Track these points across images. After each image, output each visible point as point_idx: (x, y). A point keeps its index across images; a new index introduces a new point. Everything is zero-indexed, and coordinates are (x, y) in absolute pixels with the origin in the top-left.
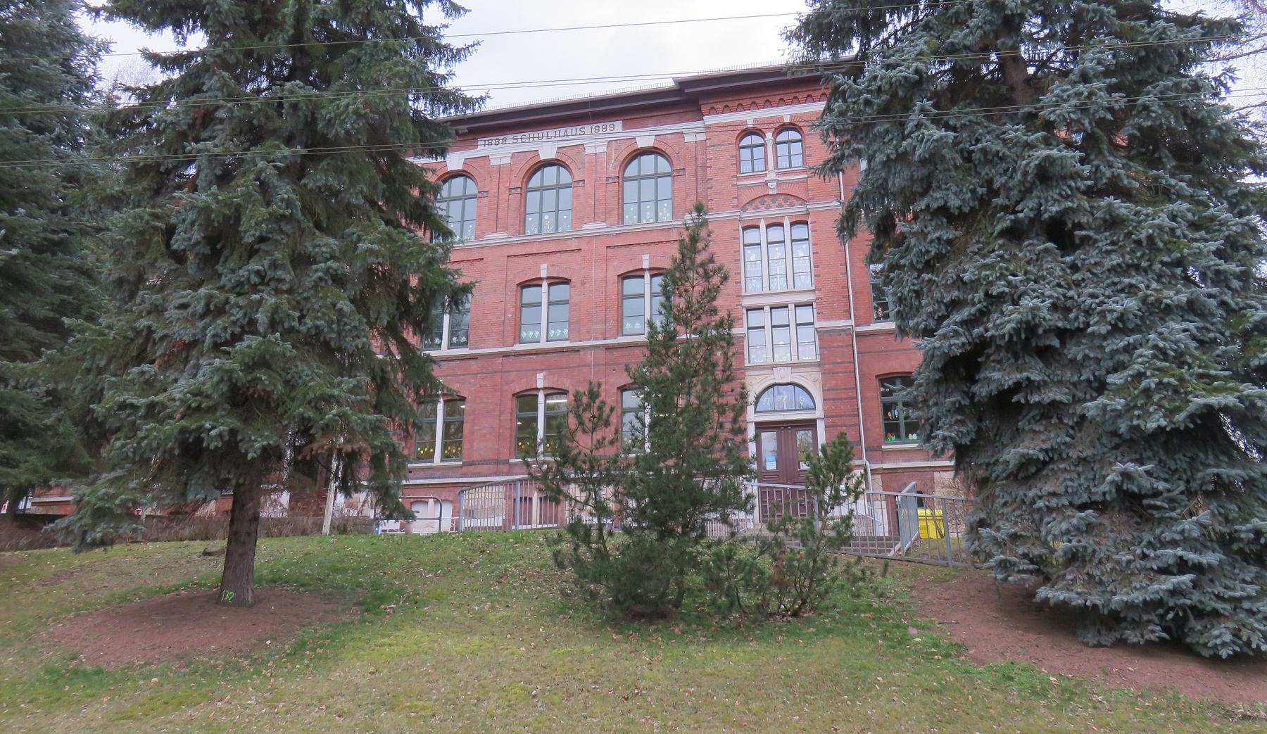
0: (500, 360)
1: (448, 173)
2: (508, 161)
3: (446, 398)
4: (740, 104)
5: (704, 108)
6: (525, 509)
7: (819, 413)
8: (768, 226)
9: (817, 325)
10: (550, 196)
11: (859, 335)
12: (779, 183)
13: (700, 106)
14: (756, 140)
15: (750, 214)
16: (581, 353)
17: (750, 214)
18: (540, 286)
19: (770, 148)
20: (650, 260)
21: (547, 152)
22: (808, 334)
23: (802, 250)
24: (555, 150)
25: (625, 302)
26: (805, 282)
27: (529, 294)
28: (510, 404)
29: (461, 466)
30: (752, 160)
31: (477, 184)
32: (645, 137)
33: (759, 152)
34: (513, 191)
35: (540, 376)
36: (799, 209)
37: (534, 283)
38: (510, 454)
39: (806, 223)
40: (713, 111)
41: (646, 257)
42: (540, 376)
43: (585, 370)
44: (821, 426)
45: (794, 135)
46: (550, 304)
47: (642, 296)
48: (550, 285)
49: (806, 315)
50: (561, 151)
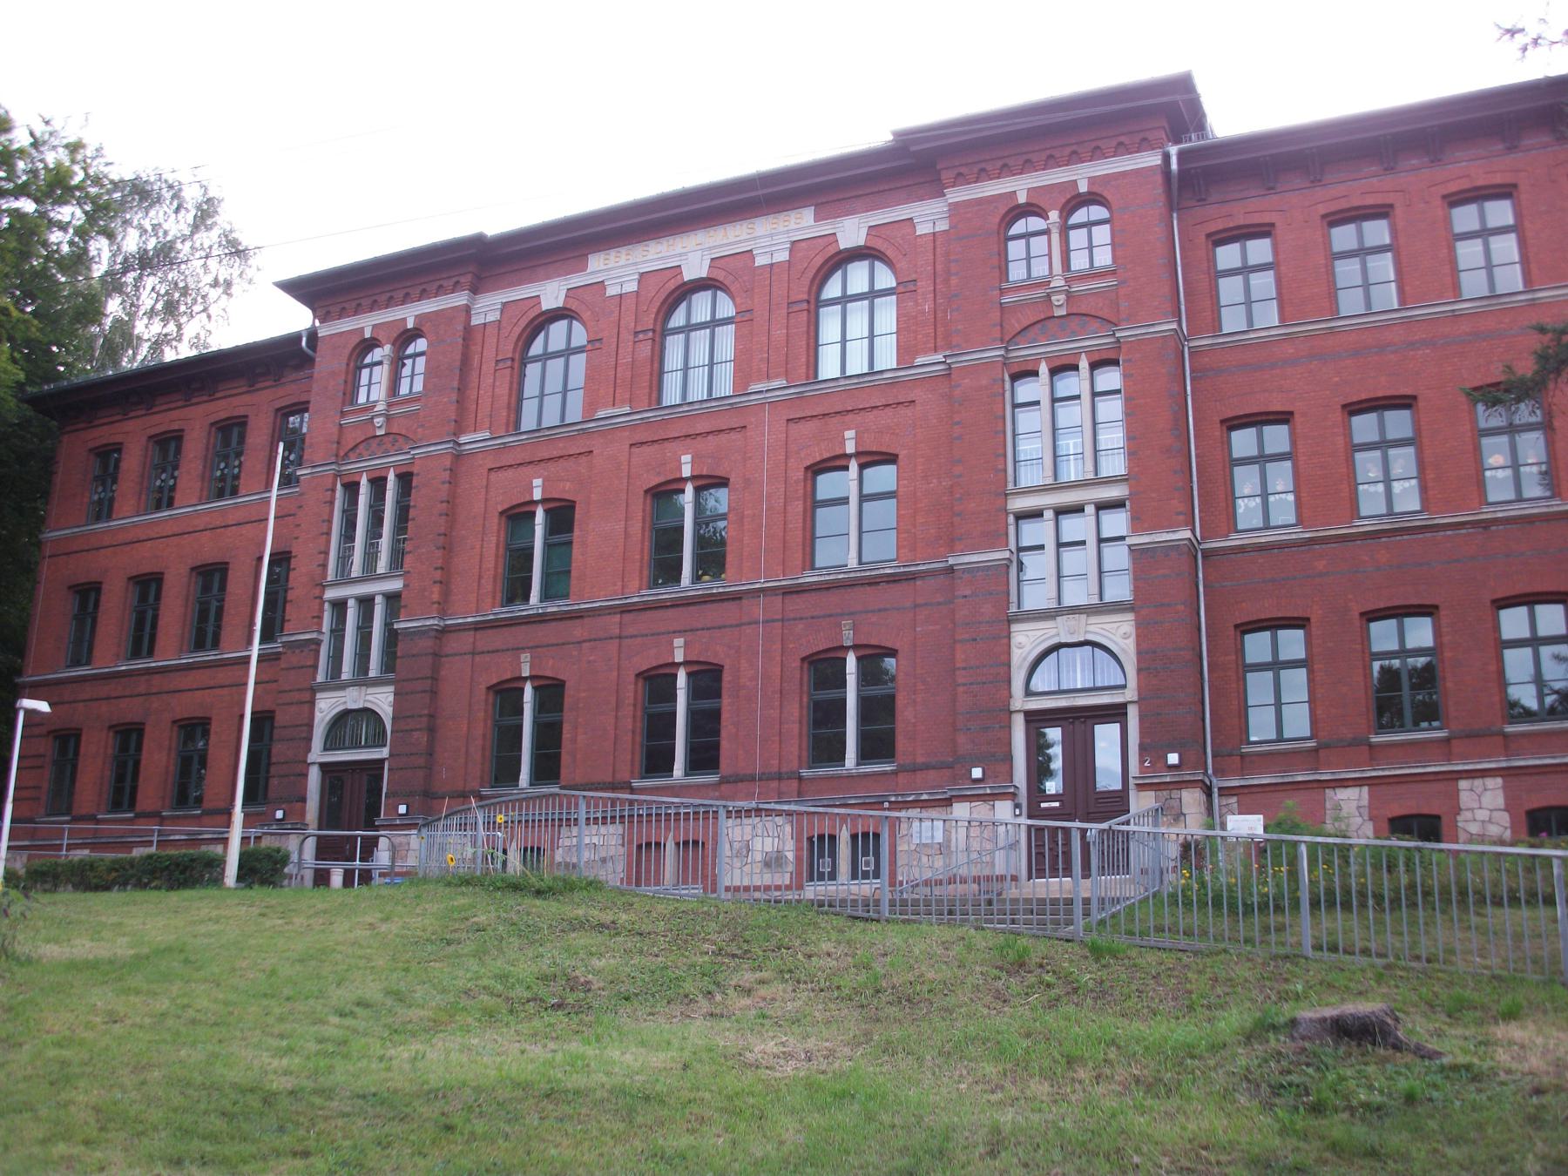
0: (617, 618)
1: (544, 313)
2: (633, 287)
3: (861, 653)
4: (1144, 139)
5: (946, 176)
6: (695, 859)
7: (1130, 694)
8: (1094, 366)
9: (1129, 541)
10: (555, 366)
11: (1207, 554)
12: (1070, 296)
13: (939, 172)
14: (1035, 223)
15: (1022, 352)
16: (744, 601)
17: (1022, 352)
18: (846, 468)
19: (1055, 237)
20: (693, 462)
21: (695, 268)
22: (1117, 557)
23: (1112, 409)
24: (864, 232)
25: (820, 512)
26: (1115, 465)
27: (828, 485)
28: (632, 692)
29: (894, 773)
30: (1091, 248)
31: (732, 297)
32: (851, 231)
33: (1039, 244)
34: (641, 336)
35: (679, 642)
36: (1098, 341)
37: (836, 463)
38: (632, 772)
39: (1115, 362)
40: (960, 179)
41: (850, 434)
42: (679, 642)
43: (748, 630)
44: (1133, 714)
45: (1098, 212)
46: (863, 498)
47: (844, 501)
48: (862, 467)
49: (1116, 523)
50: (717, 264)
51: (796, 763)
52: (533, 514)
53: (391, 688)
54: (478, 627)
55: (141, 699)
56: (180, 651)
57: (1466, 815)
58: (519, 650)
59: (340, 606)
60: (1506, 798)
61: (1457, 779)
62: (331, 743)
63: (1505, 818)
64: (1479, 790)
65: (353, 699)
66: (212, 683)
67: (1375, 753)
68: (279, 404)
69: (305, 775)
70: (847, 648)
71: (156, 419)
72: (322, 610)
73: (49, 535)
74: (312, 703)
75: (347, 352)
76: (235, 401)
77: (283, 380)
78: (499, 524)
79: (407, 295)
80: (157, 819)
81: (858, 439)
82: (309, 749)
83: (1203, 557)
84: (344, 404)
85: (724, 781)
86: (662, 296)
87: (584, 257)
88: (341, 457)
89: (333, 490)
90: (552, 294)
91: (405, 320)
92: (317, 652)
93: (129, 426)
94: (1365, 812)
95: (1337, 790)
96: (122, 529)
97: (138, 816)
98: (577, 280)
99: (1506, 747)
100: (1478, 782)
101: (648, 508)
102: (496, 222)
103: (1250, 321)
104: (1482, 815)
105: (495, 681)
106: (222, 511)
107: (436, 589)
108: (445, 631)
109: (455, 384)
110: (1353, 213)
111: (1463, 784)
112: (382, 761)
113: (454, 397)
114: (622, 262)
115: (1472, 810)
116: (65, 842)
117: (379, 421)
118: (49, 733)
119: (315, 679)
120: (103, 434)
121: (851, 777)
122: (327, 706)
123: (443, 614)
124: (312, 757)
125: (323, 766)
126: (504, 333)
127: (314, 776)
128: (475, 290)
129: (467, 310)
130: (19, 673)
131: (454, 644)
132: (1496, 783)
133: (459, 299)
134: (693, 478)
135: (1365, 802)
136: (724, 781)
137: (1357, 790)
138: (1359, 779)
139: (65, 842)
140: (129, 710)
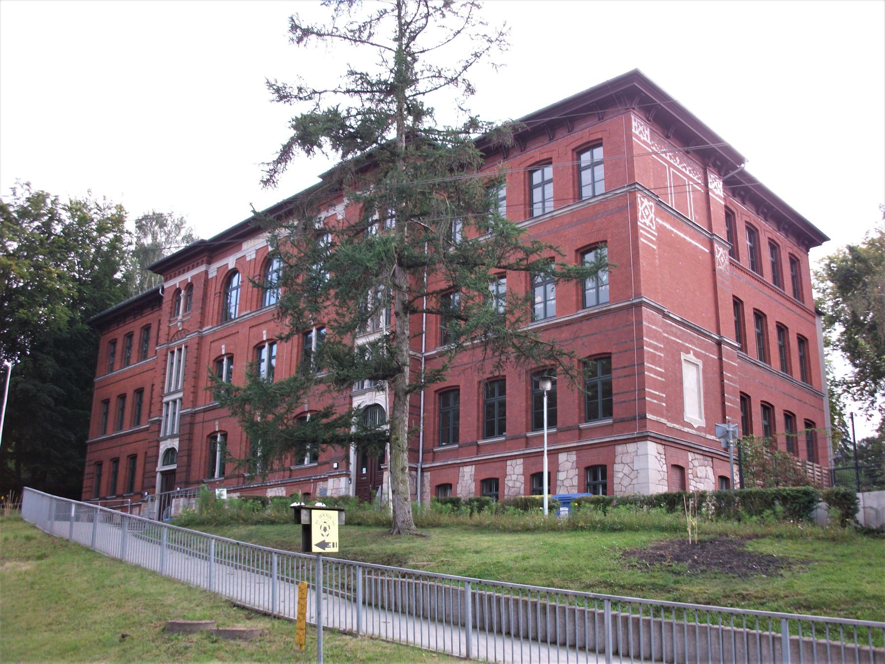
29: (504, 442)
51: (576, 419)
52: (223, 360)
53: (178, 439)
54: (205, 411)
55: (118, 448)
56: (114, 430)
57: (508, 477)
58: (215, 419)
59: (167, 404)
60: (524, 469)
61: (558, 453)
63: (522, 478)
64: (514, 465)
66: (138, 439)
67: (581, 433)
69: (155, 477)
70: (307, 412)
71: (126, 327)
72: (162, 407)
73: (96, 380)
74: (158, 446)
75: (172, 294)
76: (149, 317)
78: (253, 353)
79: (184, 270)
81: (267, 334)
82: (157, 466)
83: (425, 360)
84: (171, 317)
86: (262, 259)
87: (240, 244)
88: (169, 341)
89: (166, 355)
90: (231, 262)
91: (175, 285)
92: (160, 425)
93: (120, 330)
94: (473, 477)
95: (628, 445)
96: (116, 375)
98: (239, 255)
100: (514, 461)
101: (301, 341)
103: (544, 210)
104: (514, 477)
105: (209, 433)
106: (143, 365)
107: (192, 395)
108: (196, 413)
109: (200, 306)
110: (586, 146)
111: (509, 462)
113: (200, 311)
114: (249, 246)
115: (511, 475)
116: (546, 449)
117: (179, 324)
118: (95, 463)
119: (159, 436)
120: (110, 336)
123: (194, 406)
124: (157, 469)
125: (162, 473)
126: (257, 262)
128: (209, 263)
129: (206, 272)
130: (87, 439)
131: (199, 418)
133: (202, 268)
134: (268, 340)
135: (473, 473)
137: (470, 467)
138: (612, 441)
139: (546, 449)
140: (115, 452)
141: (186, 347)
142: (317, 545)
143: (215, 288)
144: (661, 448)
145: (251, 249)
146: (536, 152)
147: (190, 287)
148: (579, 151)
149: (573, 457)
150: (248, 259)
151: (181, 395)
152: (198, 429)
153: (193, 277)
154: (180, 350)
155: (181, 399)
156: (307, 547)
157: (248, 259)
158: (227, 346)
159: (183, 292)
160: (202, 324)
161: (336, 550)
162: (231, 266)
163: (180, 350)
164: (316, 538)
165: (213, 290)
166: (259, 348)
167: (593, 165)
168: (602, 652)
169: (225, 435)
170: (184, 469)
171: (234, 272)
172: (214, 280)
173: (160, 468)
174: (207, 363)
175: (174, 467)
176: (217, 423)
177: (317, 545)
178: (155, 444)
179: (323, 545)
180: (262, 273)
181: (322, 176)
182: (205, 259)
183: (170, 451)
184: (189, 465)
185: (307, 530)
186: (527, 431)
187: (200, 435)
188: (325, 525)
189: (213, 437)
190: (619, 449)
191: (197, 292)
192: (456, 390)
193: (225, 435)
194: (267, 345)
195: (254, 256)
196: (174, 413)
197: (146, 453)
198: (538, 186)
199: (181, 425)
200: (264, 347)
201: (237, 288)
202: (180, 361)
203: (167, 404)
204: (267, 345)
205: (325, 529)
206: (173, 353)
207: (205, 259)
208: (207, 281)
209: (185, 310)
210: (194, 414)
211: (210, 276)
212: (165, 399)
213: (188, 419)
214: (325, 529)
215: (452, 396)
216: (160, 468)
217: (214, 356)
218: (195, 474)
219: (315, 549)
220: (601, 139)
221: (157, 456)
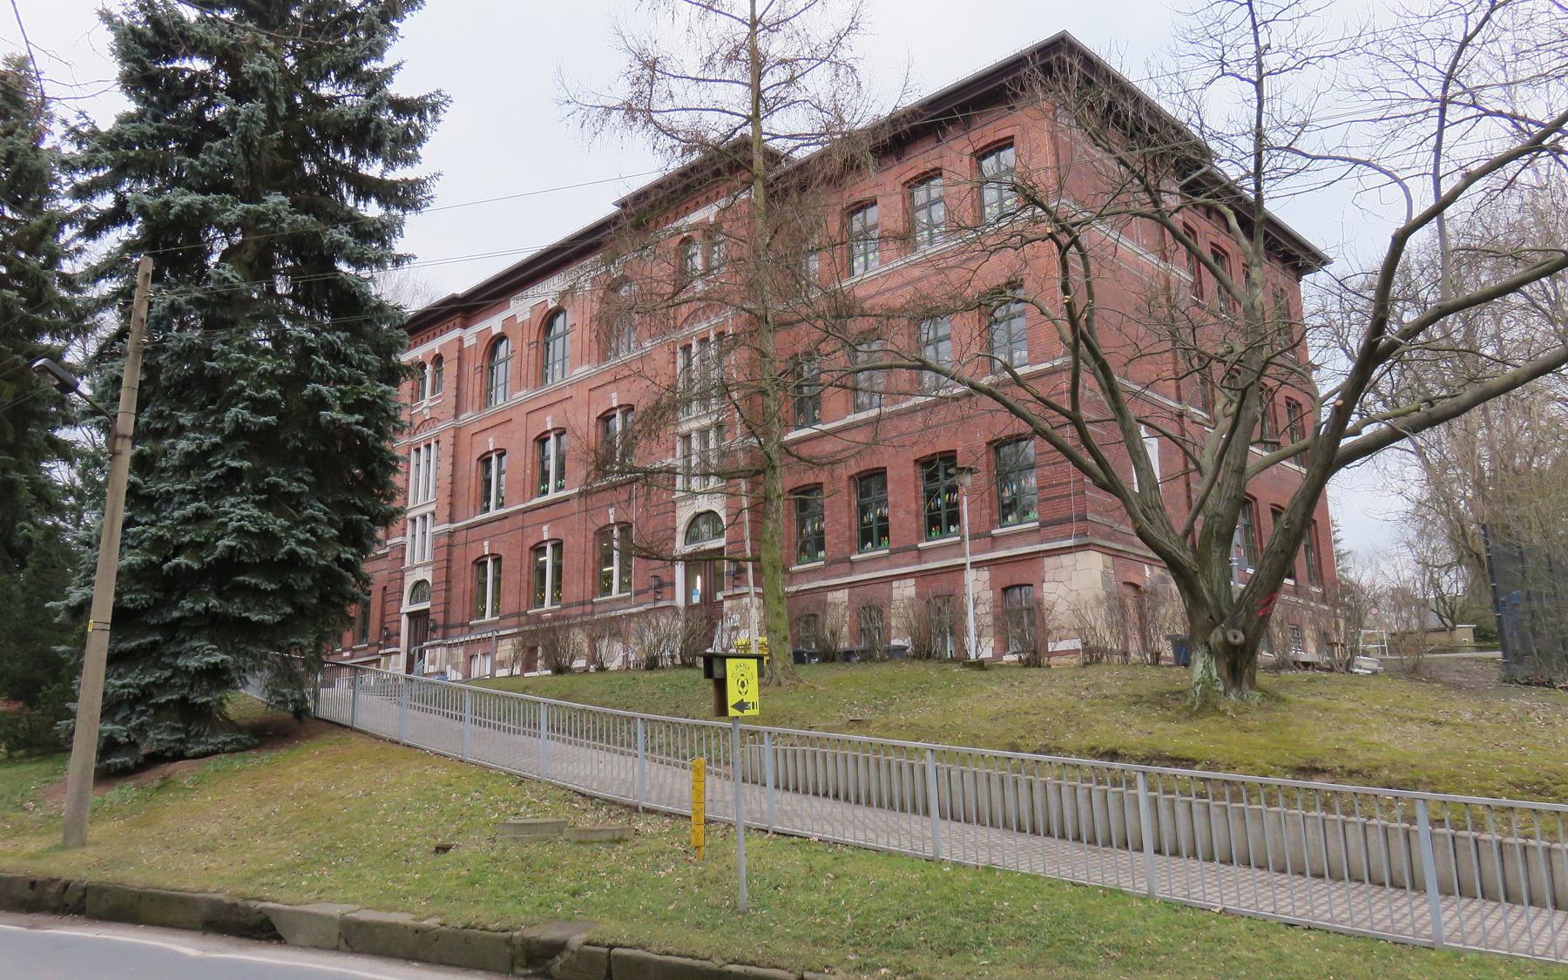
42: (611, 511)
58: (484, 539)
59: (687, 438)
62: (691, 537)
65: (703, 504)
68: (904, 179)
69: (399, 621)
74: (402, 578)
77: (973, 127)
80: (846, 567)
82: (400, 605)
85: (893, 552)
87: (508, 301)
92: (404, 549)
97: (830, 563)
99: (919, 557)
100: (902, 582)
102: (461, 287)
108: (455, 531)
111: (895, 584)
112: (722, 548)
121: (618, 600)
122: (684, 515)
124: (402, 610)
125: (411, 615)
127: (405, 620)
129: (461, 340)
131: (460, 538)
132: (911, 582)
133: (456, 333)
136: (893, 552)
141: (437, 442)
142: (734, 706)
143: (475, 362)
144: (1109, 559)
145: (523, 308)
146: (920, 159)
147: (438, 360)
148: (982, 154)
149: (985, 574)
150: (519, 320)
151: (432, 508)
152: (457, 552)
153: (441, 347)
154: (428, 446)
155: (433, 514)
156: (722, 709)
157: (519, 320)
158: (555, 417)
159: (428, 366)
160: (458, 410)
161: (756, 712)
162: (496, 330)
163: (428, 446)
164: (733, 697)
165: (472, 365)
166: (542, 440)
167: (931, 203)
168: (1417, 886)
169: (498, 560)
170: (442, 607)
171: (501, 338)
172: (473, 351)
173: (407, 607)
174: (471, 466)
175: (426, 605)
176: (486, 543)
177: (734, 706)
178: (398, 575)
179: (741, 706)
180: (541, 341)
181: (615, 204)
182: (458, 321)
183: (419, 584)
184: (447, 603)
185: (721, 685)
186: (920, 540)
187: (463, 560)
188: (743, 679)
189: (480, 563)
190: (1049, 562)
191: (450, 369)
192: (880, 473)
193: (498, 560)
194: (552, 436)
195: (528, 316)
196: (424, 533)
197: (385, 588)
198: (923, 207)
199: (436, 548)
200: (549, 438)
201: (506, 360)
202: (429, 461)
203: (414, 520)
204: (552, 436)
205: (743, 685)
206: (418, 450)
207: (458, 321)
208: (461, 350)
209: (433, 392)
210: (451, 534)
211: (466, 345)
212: (409, 515)
213: (444, 540)
214: (743, 685)
215: (874, 485)
216: (407, 607)
217: (478, 453)
218: (457, 615)
219: (732, 712)
220: (1012, 137)
221: (402, 592)
